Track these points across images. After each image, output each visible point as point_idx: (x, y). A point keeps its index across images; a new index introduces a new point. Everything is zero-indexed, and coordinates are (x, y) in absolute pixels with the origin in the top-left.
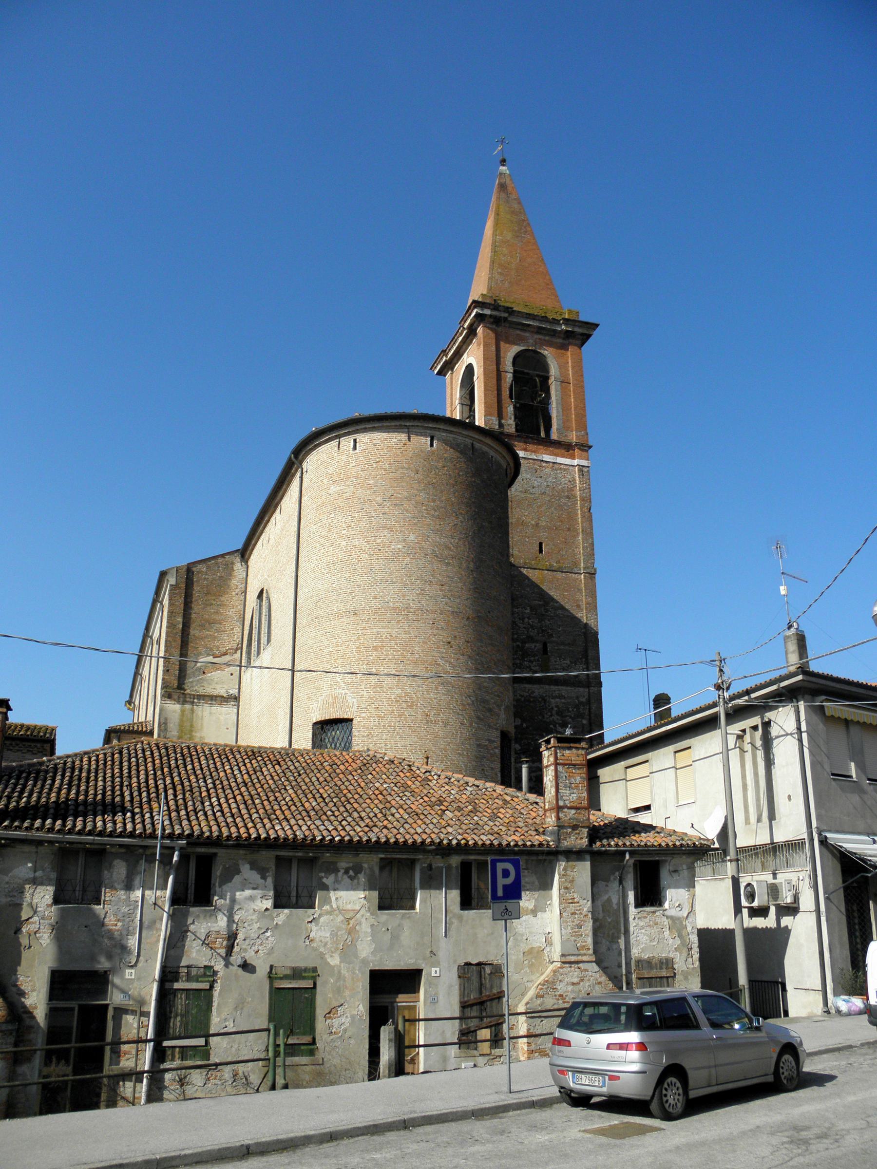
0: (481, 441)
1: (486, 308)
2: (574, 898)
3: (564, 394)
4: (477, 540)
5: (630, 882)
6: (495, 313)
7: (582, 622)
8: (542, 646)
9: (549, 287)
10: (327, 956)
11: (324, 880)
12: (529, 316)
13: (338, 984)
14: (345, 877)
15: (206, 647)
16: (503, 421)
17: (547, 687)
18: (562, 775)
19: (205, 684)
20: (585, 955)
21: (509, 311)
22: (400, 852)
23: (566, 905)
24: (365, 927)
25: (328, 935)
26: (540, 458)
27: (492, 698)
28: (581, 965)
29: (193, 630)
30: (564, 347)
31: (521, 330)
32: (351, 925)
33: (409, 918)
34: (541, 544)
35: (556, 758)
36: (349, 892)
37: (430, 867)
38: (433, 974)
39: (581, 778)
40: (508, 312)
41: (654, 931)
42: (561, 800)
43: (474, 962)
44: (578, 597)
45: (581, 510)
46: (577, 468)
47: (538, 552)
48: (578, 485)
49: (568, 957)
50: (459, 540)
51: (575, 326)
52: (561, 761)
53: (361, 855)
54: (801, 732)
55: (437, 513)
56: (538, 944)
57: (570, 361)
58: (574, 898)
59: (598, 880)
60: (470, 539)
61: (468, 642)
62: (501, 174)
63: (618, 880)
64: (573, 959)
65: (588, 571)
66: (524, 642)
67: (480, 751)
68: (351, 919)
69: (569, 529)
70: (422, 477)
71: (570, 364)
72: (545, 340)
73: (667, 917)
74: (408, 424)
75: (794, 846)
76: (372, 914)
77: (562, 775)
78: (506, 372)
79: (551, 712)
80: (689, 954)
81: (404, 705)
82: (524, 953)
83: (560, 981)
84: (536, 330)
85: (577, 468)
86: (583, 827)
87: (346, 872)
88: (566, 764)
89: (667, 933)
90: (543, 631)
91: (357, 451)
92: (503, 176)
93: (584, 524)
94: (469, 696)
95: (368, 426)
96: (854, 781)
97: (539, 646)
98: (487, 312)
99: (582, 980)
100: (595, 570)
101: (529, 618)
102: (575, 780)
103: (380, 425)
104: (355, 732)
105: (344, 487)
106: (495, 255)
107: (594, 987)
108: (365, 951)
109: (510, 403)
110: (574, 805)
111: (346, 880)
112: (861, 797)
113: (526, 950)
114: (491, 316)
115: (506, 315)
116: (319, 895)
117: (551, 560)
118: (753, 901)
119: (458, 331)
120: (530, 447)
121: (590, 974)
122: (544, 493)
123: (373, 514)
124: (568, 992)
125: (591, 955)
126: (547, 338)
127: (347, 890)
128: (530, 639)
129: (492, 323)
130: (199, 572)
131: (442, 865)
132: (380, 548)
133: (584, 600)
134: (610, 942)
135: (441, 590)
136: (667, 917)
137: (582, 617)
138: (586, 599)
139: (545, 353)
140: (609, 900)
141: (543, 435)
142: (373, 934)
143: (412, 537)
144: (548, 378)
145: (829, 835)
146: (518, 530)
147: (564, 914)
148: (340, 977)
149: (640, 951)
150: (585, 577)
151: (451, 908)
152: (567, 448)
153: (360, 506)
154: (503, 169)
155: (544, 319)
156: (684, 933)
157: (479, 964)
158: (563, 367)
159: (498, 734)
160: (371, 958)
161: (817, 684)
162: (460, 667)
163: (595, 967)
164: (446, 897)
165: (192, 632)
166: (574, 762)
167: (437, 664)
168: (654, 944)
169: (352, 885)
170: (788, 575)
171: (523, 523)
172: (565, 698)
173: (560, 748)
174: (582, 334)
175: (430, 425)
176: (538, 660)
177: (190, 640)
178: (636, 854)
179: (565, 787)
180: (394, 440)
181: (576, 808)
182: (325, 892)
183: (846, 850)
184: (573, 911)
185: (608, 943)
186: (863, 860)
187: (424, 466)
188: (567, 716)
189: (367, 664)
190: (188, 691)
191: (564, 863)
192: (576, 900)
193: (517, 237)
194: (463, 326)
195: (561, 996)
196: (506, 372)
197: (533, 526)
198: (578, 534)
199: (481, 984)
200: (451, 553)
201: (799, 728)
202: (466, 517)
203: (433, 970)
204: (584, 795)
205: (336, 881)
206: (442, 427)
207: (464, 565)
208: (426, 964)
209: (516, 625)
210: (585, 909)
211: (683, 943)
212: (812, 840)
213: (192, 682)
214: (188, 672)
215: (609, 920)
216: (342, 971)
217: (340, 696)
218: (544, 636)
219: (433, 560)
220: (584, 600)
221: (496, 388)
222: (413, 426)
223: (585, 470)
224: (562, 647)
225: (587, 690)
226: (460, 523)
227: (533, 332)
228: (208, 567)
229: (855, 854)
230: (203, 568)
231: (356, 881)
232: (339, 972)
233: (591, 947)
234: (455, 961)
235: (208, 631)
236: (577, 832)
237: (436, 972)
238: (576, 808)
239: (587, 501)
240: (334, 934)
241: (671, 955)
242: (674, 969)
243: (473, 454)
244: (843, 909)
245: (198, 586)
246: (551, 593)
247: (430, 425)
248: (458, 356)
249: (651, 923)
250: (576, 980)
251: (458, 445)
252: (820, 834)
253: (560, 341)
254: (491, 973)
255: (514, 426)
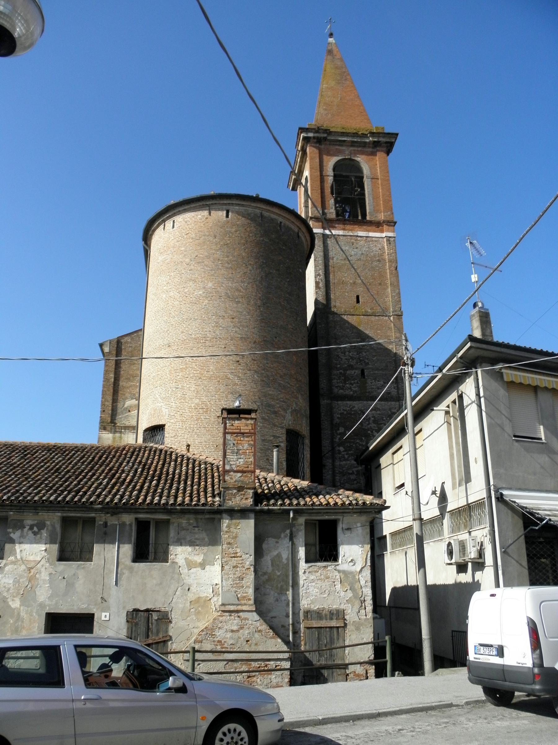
0: (269, 210)
1: (310, 132)
2: (237, 553)
3: (374, 187)
4: (264, 284)
5: (300, 539)
6: (316, 135)
7: (393, 352)
8: (360, 372)
9: (362, 114)
10: (9, 600)
11: (12, 535)
12: (343, 134)
13: (16, 625)
14: (30, 532)
15: (130, 393)
16: (326, 211)
17: (365, 402)
18: (230, 442)
19: (130, 419)
20: (245, 604)
21: (328, 132)
22: (75, 511)
23: (228, 559)
24: (44, 576)
25: (11, 582)
26: (356, 234)
27: (278, 403)
28: (241, 614)
29: (122, 382)
30: (373, 154)
31: (339, 145)
32: (32, 574)
33: (83, 568)
34: (358, 297)
35: (225, 428)
36: (32, 545)
37: (105, 525)
38: (103, 618)
39: (249, 445)
40: (327, 133)
41: (326, 584)
42: (228, 464)
43: (142, 608)
44: (389, 333)
45: (389, 269)
46: (385, 239)
47: (356, 302)
48: (386, 251)
49: (227, 607)
50: (248, 283)
51: (379, 137)
52: (230, 431)
53: (40, 514)
54: (480, 398)
55: (230, 266)
56: (205, 595)
57: (378, 163)
58: (237, 553)
59: (268, 537)
60: (257, 283)
61: (254, 360)
62: (329, 43)
63: (288, 537)
64: (232, 608)
65: (396, 313)
66: (345, 370)
67: (264, 445)
68: (32, 568)
69: (380, 284)
70: (219, 240)
71: (378, 165)
72: (358, 150)
73: (339, 571)
74: (208, 203)
75: (479, 504)
76: (51, 564)
77: (230, 442)
78: (328, 176)
79: (369, 421)
80: (361, 606)
81: (201, 411)
82: (191, 602)
83: (219, 628)
84: (350, 144)
85: (385, 239)
86: (249, 488)
87: (31, 528)
88: (234, 433)
89: (338, 586)
90: (361, 361)
91: (175, 229)
92: (330, 45)
93: (392, 279)
94: (255, 402)
95: (181, 209)
96: (543, 443)
97: (358, 372)
98: (311, 135)
99: (242, 628)
100: (402, 312)
101: (349, 352)
102: (243, 447)
103: (189, 207)
104: (166, 435)
105: (166, 256)
106: (321, 98)
107: (253, 635)
108: (43, 597)
109: (331, 197)
110: (241, 469)
111: (30, 534)
112: (550, 457)
113: (193, 599)
114: (314, 137)
115: (325, 135)
116: (8, 546)
117: (366, 308)
118: (452, 558)
119: (296, 154)
120: (348, 227)
121: (250, 622)
122: (360, 260)
123: (183, 271)
124: (227, 638)
125: (252, 605)
126: (359, 149)
127: (31, 543)
128: (351, 367)
129: (316, 143)
130: (126, 342)
131: (117, 523)
132: (186, 295)
133: (393, 335)
134: (279, 594)
135: (232, 322)
136: (339, 571)
137: (393, 348)
138: (395, 334)
139: (358, 159)
140: (279, 556)
141: (360, 218)
142: (51, 581)
143: (210, 285)
144: (363, 177)
145: (505, 492)
146: (339, 288)
147: (226, 567)
148: (19, 618)
149: (309, 602)
150: (393, 318)
151: (123, 560)
152: (378, 225)
153: (175, 268)
154: (331, 40)
155: (355, 135)
156: (357, 586)
157: (147, 611)
158: (372, 168)
159: (284, 431)
160: (47, 602)
161: (501, 352)
162: (247, 379)
163: (256, 616)
164: (118, 551)
165: (121, 383)
166: (242, 431)
167: (227, 378)
168: (325, 596)
169: (35, 538)
170: (478, 264)
171: (343, 283)
172: (379, 410)
173: (229, 419)
174: (386, 143)
175: (225, 202)
176: (357, 383)
177: (120, 389)
178: (304, 513)
179: (233, 452)
180: (199, 216)
181: (243, 472)
182: (12, 545)
183: (518, 505)
184: (235, 564)
185: (276, 594)
186: (532, 514)
187: (221, 232)
188: (382, 424)
189: (176, 382)
190: (118, 424)
191: (227, 521)
192: (238, 555)
193: (339, 83)
194: (298, 150)
195: (219, 641)
196: (328, 176)
197: (351, 284)
198: (387, 287)
199: (148, 629)
200: (241, 294)
201: (478, 395)
202: (255, 266)
203: (104, 614)
204: (251, 460)
205: (22, 536)
206: (234, 202)
207: (252, 302)
208: (97, 609)
209: (339, 357)
210: (248, 563)
211: (355, 596)
212: (490, 497)
213: (121, 418)
214: (118, 411)
215: (279, 574)
216: (21, 614)
217: (158, 408)
218: (361, 364)
219: (226, 300)
220: (393, 335)
221: (320, 187)
222: (212, 204)
223: (392, 239)
224: (376, 372)
225: (398, 403)
226: (249, 272)
227: (347, 146)
228: (132, 339)
229: (526, 508)
230: (128, 339)
231: (39, 536)
232: (19, 614)
233: (252, 598)
234: (124, 608)
235: (132, 382)
236: (243, 493)
237: (106, 616)
238: (243, 472)
239: (393, 262)
240: (16, 581)
241: (342, 607)
242: (345, 619)
243: (262, 220)
244: (525, 563)
245: (126, 352)
246: (367, 332)
247: (225, 202)
248: (301, 174)
249: (322, 577)
250: (235, 628)
251: (249, 215)
252: (496, 491)
253: (370, 150)
254: (158, 619)
255: (334, 213)
